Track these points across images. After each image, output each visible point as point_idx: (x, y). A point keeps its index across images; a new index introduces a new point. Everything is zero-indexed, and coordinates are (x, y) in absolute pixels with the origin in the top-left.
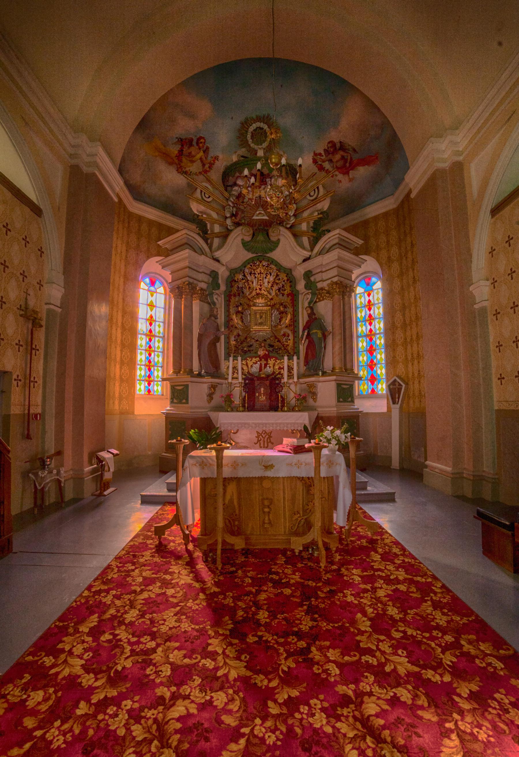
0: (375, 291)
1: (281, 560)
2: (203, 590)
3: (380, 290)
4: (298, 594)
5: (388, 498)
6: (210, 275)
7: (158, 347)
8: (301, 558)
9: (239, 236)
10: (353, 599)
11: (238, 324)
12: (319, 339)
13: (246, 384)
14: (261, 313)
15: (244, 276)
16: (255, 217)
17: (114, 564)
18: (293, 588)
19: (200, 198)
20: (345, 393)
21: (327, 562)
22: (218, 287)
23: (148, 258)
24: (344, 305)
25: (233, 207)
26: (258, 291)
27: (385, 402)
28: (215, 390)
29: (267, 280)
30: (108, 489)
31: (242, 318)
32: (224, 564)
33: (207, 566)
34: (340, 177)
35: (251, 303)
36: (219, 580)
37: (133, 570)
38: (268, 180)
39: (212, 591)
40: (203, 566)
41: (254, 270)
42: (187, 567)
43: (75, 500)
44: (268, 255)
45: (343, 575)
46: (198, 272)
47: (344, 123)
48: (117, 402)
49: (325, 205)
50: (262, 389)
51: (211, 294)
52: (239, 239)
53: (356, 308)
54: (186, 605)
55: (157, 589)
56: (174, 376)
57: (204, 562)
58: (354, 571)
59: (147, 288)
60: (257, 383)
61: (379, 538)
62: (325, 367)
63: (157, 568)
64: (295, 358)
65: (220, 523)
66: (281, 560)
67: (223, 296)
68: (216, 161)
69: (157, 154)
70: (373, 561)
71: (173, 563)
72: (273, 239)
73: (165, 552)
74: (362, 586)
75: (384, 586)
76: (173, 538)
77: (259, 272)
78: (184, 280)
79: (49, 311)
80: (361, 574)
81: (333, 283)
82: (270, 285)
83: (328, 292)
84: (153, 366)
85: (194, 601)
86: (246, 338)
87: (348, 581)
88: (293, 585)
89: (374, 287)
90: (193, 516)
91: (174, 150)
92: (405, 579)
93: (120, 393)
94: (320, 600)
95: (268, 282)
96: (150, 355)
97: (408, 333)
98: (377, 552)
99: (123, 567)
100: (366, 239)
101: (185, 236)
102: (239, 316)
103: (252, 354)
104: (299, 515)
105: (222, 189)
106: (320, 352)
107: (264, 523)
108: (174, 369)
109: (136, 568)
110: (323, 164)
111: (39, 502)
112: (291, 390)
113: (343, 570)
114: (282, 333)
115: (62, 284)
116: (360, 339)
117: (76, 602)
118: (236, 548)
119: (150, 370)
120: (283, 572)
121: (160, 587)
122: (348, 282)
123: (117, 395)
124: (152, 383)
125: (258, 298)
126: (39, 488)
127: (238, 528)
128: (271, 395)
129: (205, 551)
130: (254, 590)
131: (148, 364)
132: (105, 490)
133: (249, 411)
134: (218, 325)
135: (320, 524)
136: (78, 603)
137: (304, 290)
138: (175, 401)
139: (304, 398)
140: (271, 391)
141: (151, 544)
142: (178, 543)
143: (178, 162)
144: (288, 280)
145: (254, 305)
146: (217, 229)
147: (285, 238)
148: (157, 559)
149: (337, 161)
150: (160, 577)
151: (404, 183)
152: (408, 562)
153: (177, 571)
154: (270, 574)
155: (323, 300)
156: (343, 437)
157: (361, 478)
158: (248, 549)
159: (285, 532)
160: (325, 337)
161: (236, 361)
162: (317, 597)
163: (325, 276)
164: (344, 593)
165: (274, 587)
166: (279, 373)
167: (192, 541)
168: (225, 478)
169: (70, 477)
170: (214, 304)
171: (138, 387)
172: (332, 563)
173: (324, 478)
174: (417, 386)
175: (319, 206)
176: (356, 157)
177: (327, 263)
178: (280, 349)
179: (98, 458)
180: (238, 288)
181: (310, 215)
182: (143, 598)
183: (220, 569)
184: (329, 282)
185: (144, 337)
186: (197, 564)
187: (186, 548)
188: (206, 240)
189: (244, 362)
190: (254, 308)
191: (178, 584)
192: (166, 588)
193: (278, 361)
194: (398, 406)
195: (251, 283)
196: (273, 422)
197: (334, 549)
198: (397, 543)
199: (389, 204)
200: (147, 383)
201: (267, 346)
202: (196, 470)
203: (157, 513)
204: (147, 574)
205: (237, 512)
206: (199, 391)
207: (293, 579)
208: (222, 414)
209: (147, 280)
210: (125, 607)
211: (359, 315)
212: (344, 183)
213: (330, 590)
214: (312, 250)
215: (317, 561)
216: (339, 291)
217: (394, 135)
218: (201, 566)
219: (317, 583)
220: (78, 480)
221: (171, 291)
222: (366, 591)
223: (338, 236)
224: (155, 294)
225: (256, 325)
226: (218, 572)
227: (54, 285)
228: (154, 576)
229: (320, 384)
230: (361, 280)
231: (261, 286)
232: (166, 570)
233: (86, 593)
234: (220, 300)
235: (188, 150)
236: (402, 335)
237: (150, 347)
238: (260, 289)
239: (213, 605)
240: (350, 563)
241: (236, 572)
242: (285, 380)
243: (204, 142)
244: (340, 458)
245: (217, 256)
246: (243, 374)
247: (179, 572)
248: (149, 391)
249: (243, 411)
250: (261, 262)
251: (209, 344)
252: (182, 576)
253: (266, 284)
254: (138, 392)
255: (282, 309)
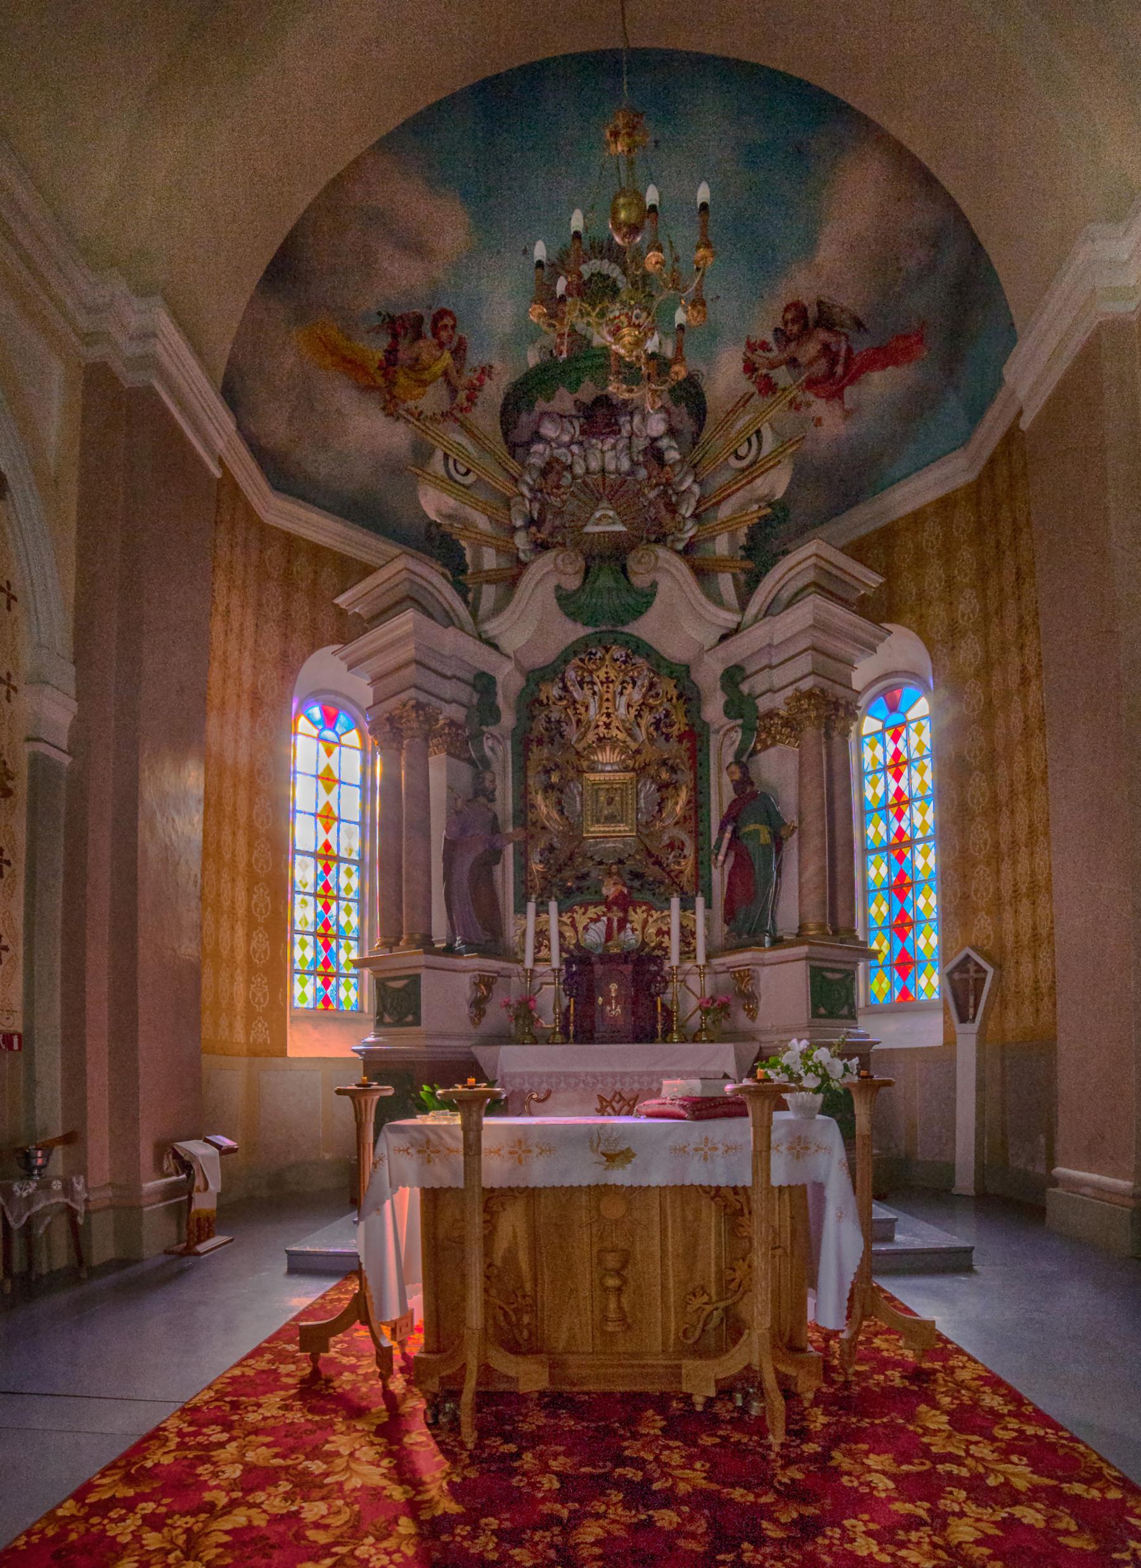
0: (913, 725)
1: (653, 1424)
2: (413, 1508)
3: (926, 723)
4: (701, 1526)
5: (953, 1263)
6: (474, 686)
7: (349, 888)
8: (709, 1420)
9: (548, 575)
10: (875, 1549)
11: (548, 817)
12: (761, 851)
13: (571, 975)
14: (610, 787)
15: (565, 688)
16: (590, 529)
17: (173, 1424)
18: (686, 1509)
19: (446, 476)
20: (832, 996)
21: (788, 1432)
22: (494, 715)
23: (314, 647)
24: (829, 756)
25: (531, 501)
26: (602, 731)
27: (939, 1018)
28: (489, 990)
29: (624, 699)
30: (208, 1237)
31: (559, 803)
32: (484, 1433)
33: (434, 1436)
34: (819, 407)
35: (585, 764)
36: (465, 1479)
37: (221, 1445)
38: (622, 420)
39: (439, 1512)
40: (424, 1439)
41: (591, 672)
42: (377, 1440)
43: (121, 1263)
44: (626, 629)
45: (838, 1472)
46: (444, 676)
47: (828, 253)
48: (239, 1025)
49: (777, 482)
50: (614, 987)
51: (477, 736)
52: (552, 581)
53: (862, 774)
54: (352, 1554)
55: (277, 1502)
56: (386, 953)
57: (429, 1426)
58: (873, 1461)
59: (315, 733)
60: (599, 969)
61: (938, 1365)
62: (780, 925)
63: (291, 1441)
64: (700, 901)
65: (475, 1318)
66: (653, 1424)
67: (509, 743)
68: (487, 381)
69: (329, 360)
70: (926, 1430)
71: (340, 1427)
72: (640, 581)
73: (323, 1397)
74: (902, 1507)
75: (971, 1509)
76: (353, 1360)
77: (603, 676)
78: (404, 696)
79: (36, 761)
80: (893, 1469)
81: (800, 696)
82: (633, 712)
83: (787, 723)
84: (337, 937)
85: (378, 1540)
86: (571, 858)
87: (856, 1490)
88: (686, 1500)
89: (911, 715)
90: (404, 1298)
91: (374, 348)
92: (1035, 1489)
93: (248, 1002)
94: (768, 1550)
95: (629, 706)
96: (327, 908)
97: (1005, 828)
98: (935, 1405)
99: (195, 1434)
100: (890, 573)
101: (404, 574)
102: (554, 796)
103: (588, 897)
104: (705, 1298)
105: (502, 450)
106: (767, 883)
107: (605, 1319)
108: (383, 936)
109: (232, 1439)
110: (772, 373)
111: (17, 1267)
112: (690, 988)
113: (837, 1455)
114: (666, 839)
115: (73, 692)
116: (872, 858)
117: (29, 1533)
118: (523, 1388)
119: (327, 946)
120: (657, 1459)
121: (288, 1497)
122: (840, 691)
123: (240, 1005)
124: (333, 981)
125: (603, 749)
126: (15, 1226)
127: (530, 1334)
128: (635, 1002)
129: (436, 1395)
130: (565, 1513)
131: (321, 930)
132: (199, 1242)
133: (578, 1041)
134: (495, 817)
135: (767, 1322)
136: (35, 1539)
137: (725, 720)
138: (387, 1019)
139: (724, 1006)
140: (637, 991)
141: (288, 1375)
142: (365, 1375)
143: (386, 382)
144: (679, 697)
145: (593, 770)
146: (490, 560)
147: (666, 574)
148: (297, 1417)
149: (811, 363)
150: (294, 1467)
151: (1002, 395)
152: (1036, 1436)
153: (345, 1451)
154: (617, 1466)
155: (773, 745)
156: (839, 1065)
157: (881, 1212)
158: (560, 1394)
159: (664, 1343)
160: (778, 842)
161: (544, 916)
162: (759, 1541)
163: (779, 677)
164: (844, 1529)
165: (627, 1505)
166: (659, 946)
167: (402, 1370)
168: (492, 1190)
169: (107, 1202)
170: (486, 763)
171: (297, 990)
172: (804, 1435)
173: (780, 1188)
174: (1027, 969)
175: (762, 486)
176: (862, 345)
177: (783, 637)
178: (662, 883)
179: (176, 1155)
180: (549, 721)
181: (738, 510)
182: (229, 1527)
183: (470, 1446)
184: (789, 692)
185: (310, 861)
186: (408, 1432)
187: (385, 1386)
188: (462, 590)
189: (566, 918)
190: (592, 777)
191: (341, 1490)
192: (305, 1499)
193: (656, 915)
194: (973, 1027)
195: (583, 710)
196: (639, 1069)
197: (810, 1395)
198: (994, 1382)
199: (952, 473)
200: (319, 980)
201: (626, 877)
202: (409, 1165)
203: (323, 1297)
204: (260, 1455)
205: (528, 1286)
206: (447, 993)
207: (686, 1480)
208: (505, 1049)
209: (316, 712)
210: (168, 1552)
211: (869, 793)
212: (829, 424)
213: (801, 1516)
214: (743, 606)
215: (760, 1428)
216: (818, 717)
217: (977, 248)
218: (418, 1438)
219: (758, 1496)
220: (127, 1208)
221: (372, 731)
222: (914, 1523)
223: (813, 560)
224: (336, 749)
225: (598, 822)
226: (465, 1454)
227: (48, 690)
228: (278, 1462)
229: (766, 970)
230: (874, 698)
231: (608, 715)
232: (316, 1448)
233: (69, 1508)
234: (499, 750)
235: (410, 346)
236: (987, 835)
237: (327, 887)
238: (607, 726)
239: (436, 1555)
240: (857, 1435)
241: (518, 1456)
242: (675, 960)
243: (454, 327)
244: (829, 1132)
245: (491, 634)
246: (562, 949)
247: (351, 1454)
248: (326, 1001)
249: (562, 1043)
250: (607, 650)
251: (471, 871)
252: (357, 1462)
253: (622, 710)
254: (297, 1004)
255: (665, 776)
